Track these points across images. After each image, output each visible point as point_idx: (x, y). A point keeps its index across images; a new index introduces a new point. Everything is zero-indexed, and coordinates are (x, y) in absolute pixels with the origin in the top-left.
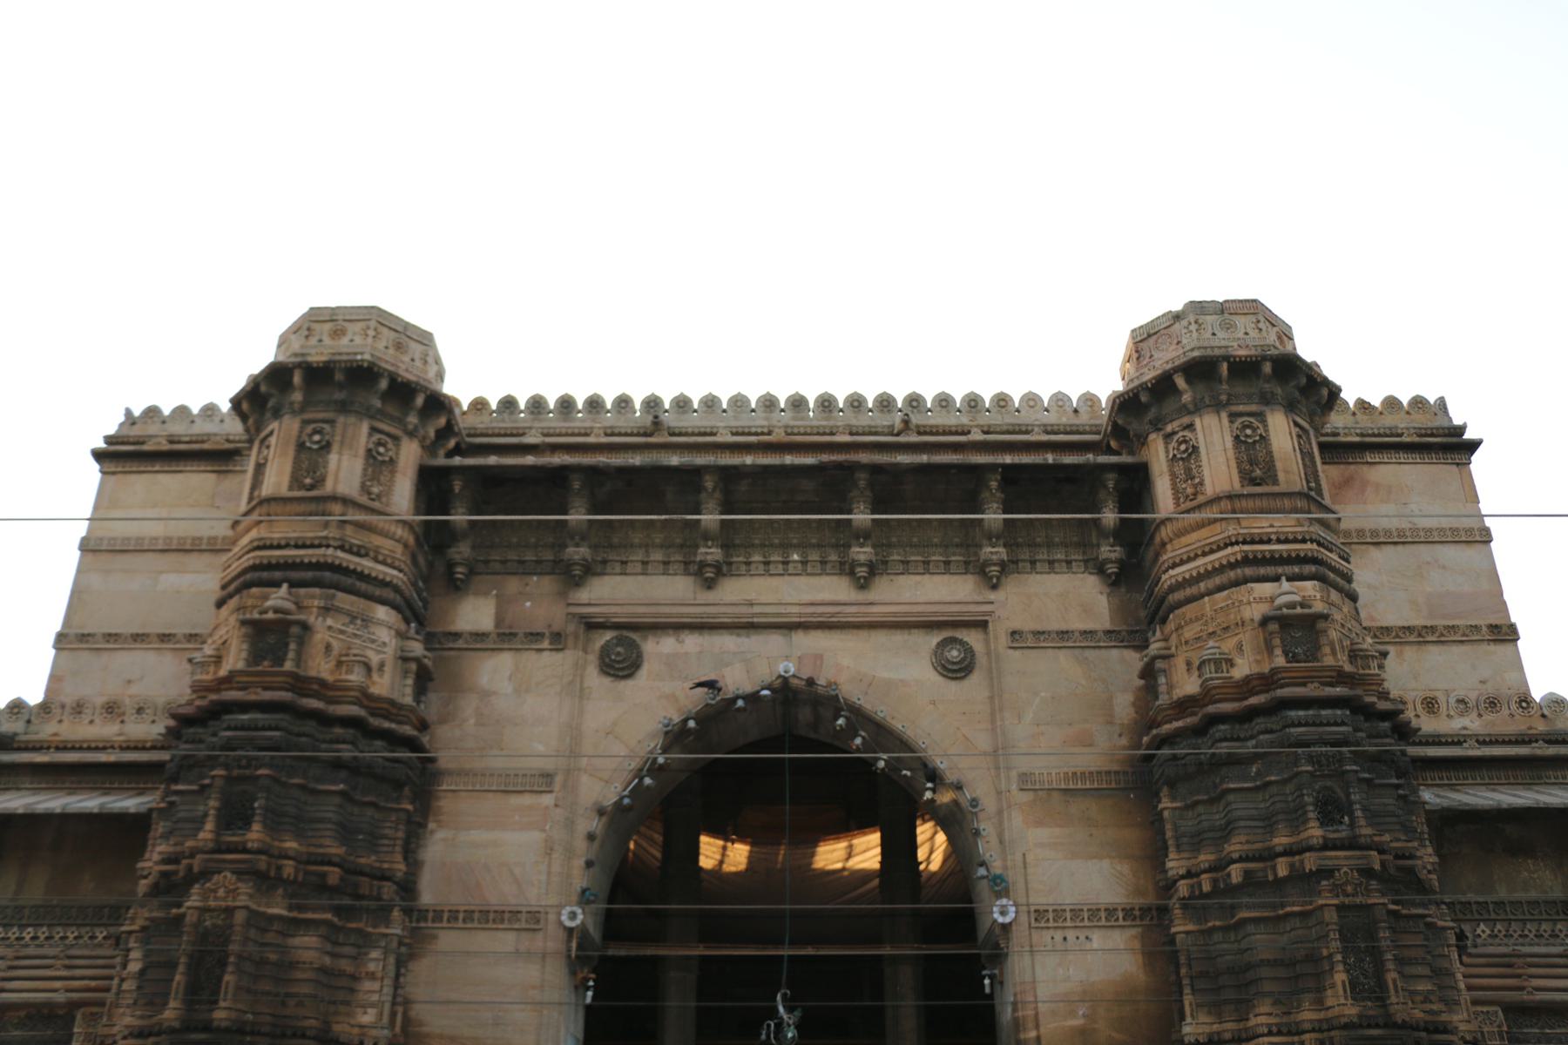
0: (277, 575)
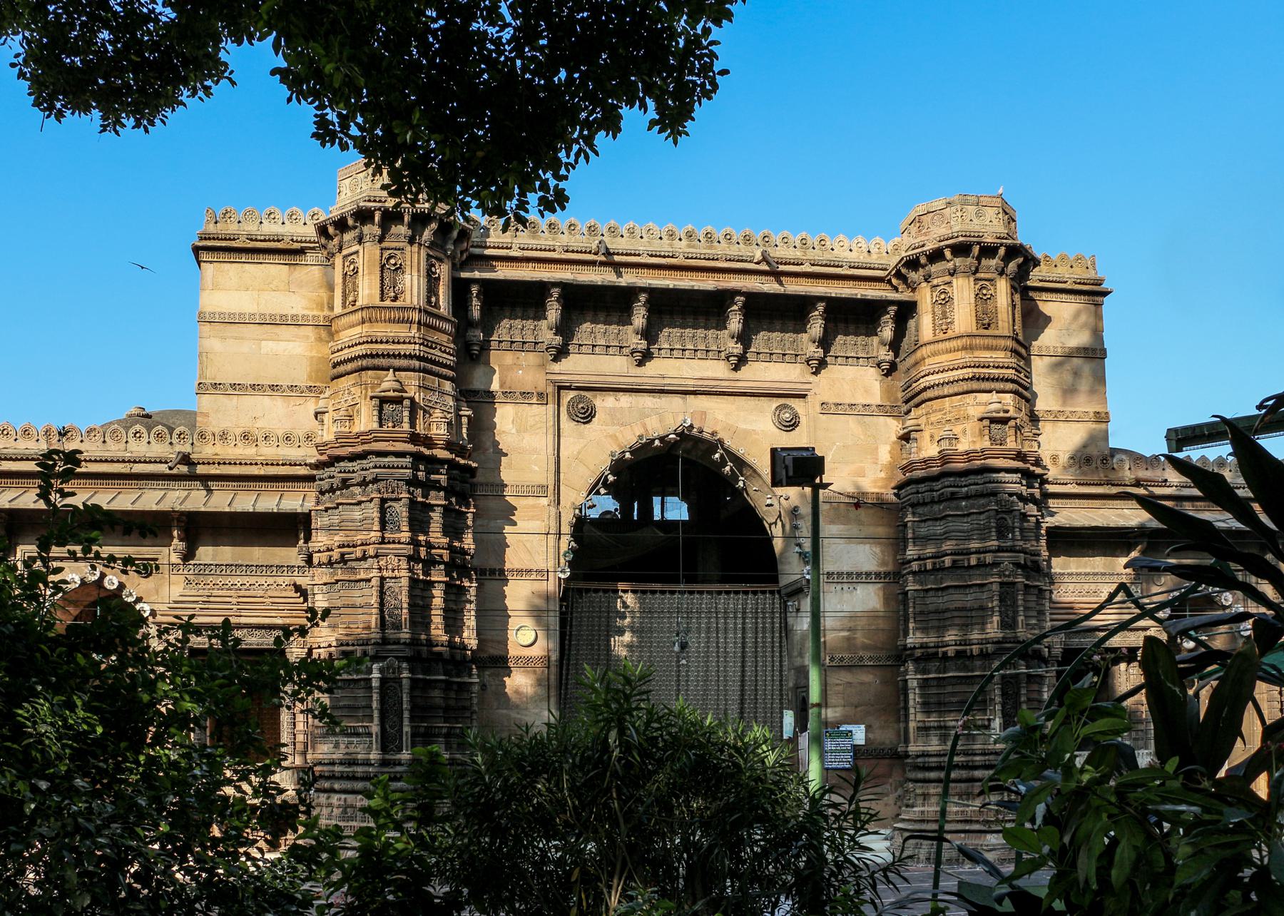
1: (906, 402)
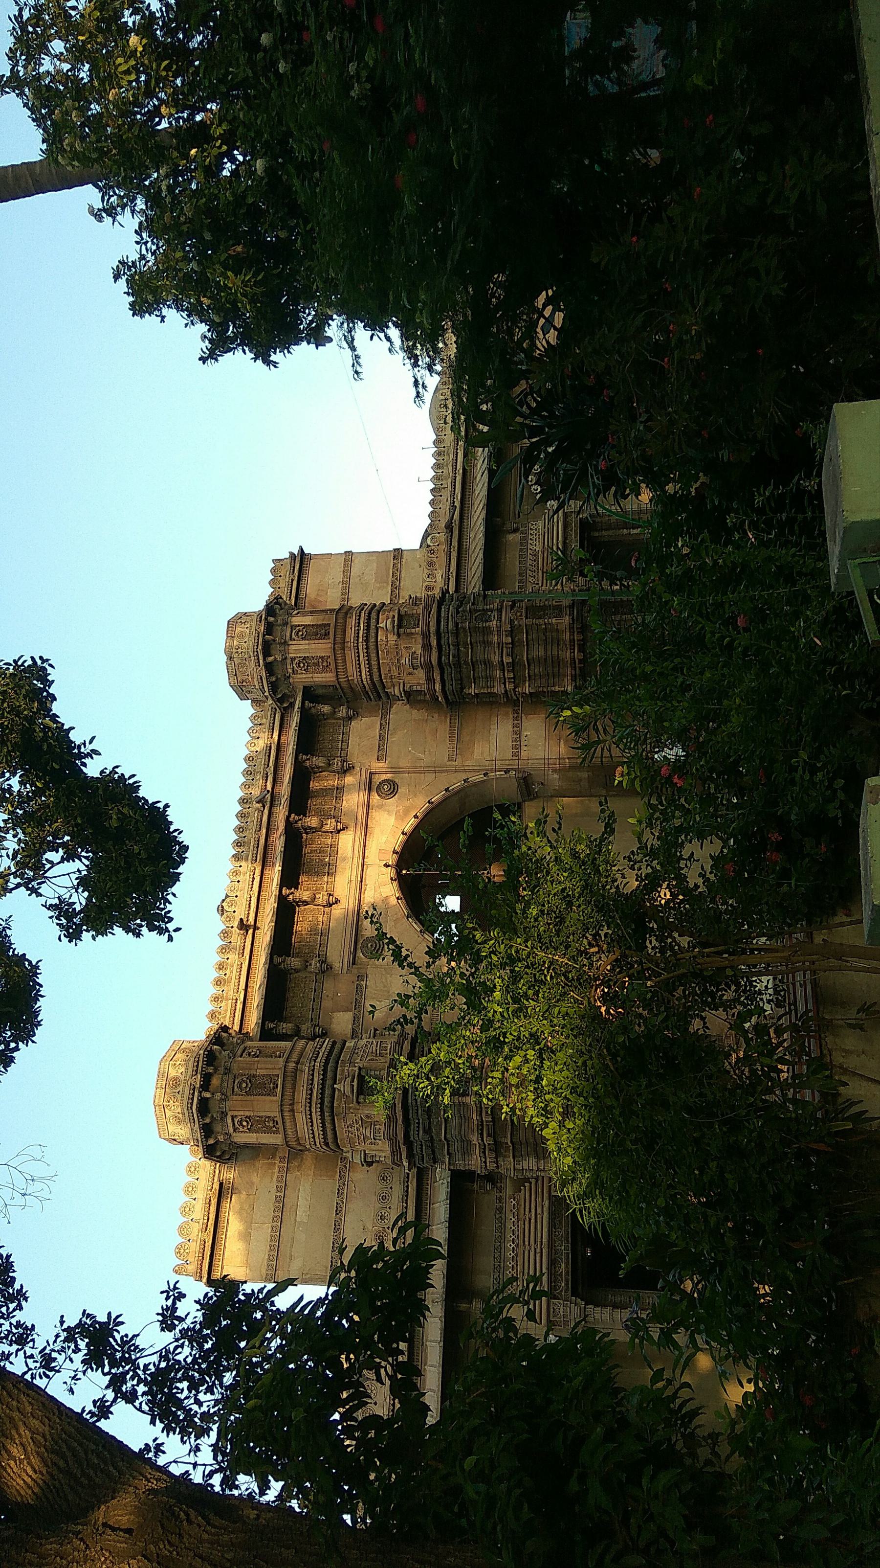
0: (328, 1092)
1: (380, 697)
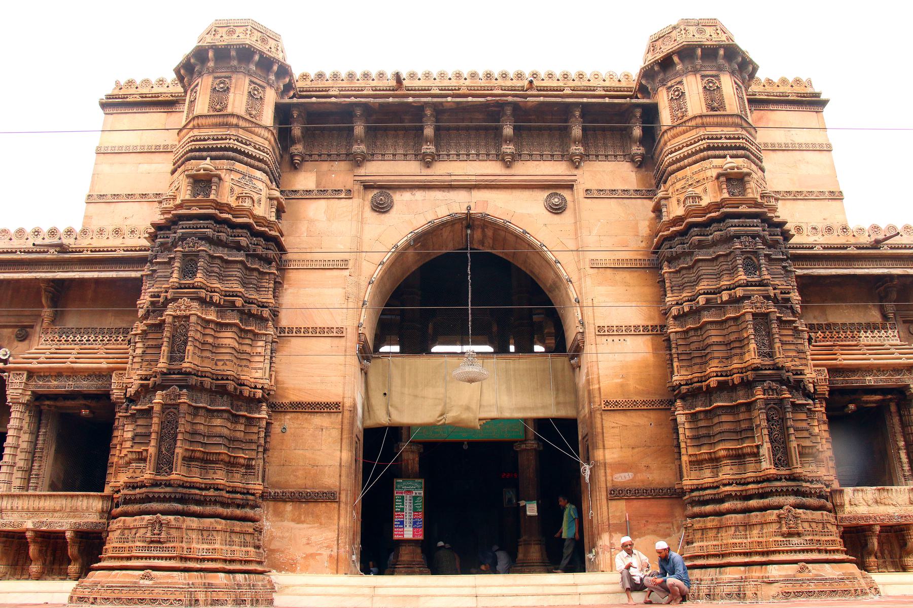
0: (205, 154)
